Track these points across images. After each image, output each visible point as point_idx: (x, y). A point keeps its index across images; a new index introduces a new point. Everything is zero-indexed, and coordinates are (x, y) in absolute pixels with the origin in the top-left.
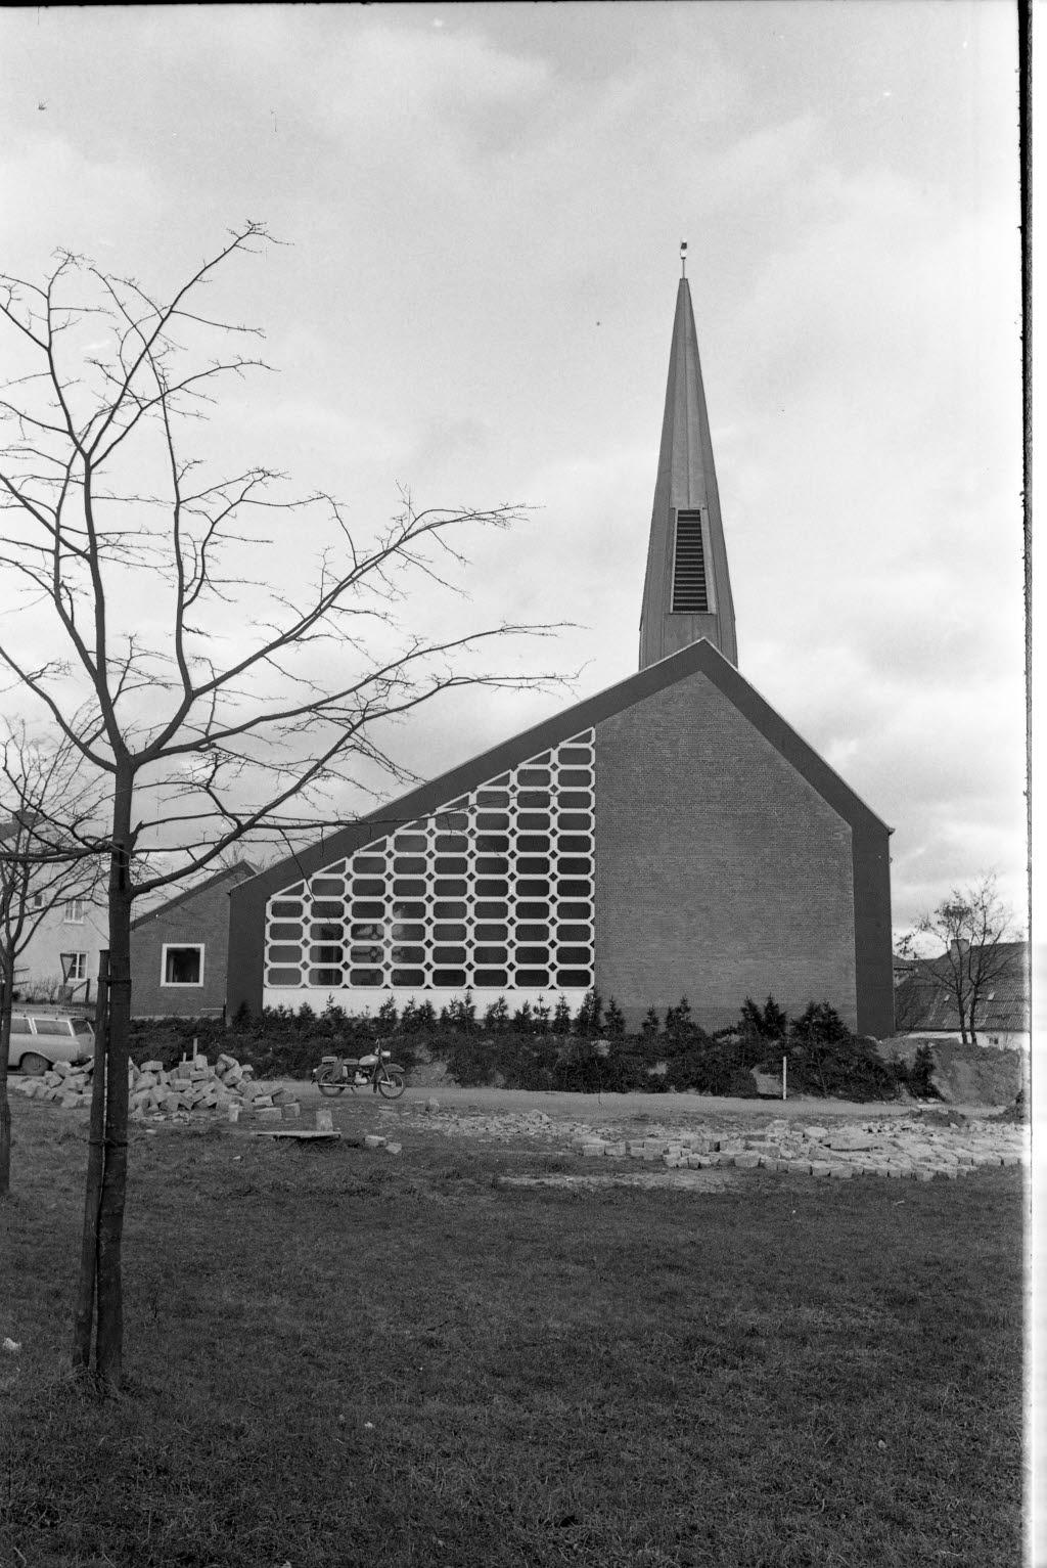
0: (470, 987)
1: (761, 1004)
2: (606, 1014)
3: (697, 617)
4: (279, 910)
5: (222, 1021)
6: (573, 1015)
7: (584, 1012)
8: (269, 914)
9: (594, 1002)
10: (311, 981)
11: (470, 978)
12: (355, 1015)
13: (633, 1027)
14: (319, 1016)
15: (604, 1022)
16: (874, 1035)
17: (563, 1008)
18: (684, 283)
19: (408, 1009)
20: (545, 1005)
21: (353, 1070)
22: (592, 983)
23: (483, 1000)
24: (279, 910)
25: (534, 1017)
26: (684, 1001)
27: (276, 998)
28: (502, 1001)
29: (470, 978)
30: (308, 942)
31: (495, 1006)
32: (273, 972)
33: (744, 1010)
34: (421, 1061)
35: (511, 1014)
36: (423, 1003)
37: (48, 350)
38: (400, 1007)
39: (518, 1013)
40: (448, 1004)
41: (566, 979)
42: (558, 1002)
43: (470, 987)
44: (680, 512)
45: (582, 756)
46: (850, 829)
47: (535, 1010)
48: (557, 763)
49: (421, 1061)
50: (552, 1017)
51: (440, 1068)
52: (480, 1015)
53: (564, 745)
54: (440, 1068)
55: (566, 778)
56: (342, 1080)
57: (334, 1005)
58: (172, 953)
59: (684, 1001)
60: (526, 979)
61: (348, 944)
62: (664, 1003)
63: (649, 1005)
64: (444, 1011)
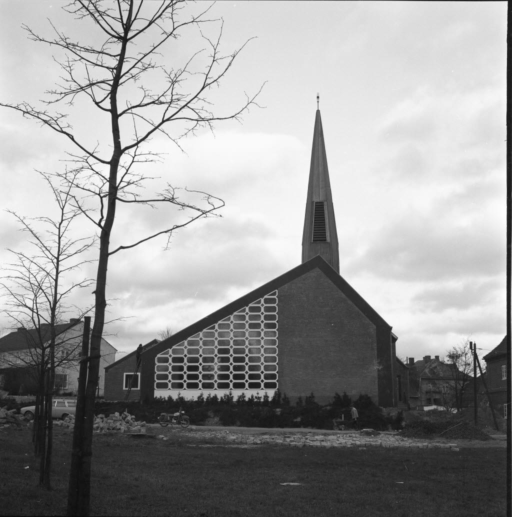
0: (231, 389)
1: (342, 394)
2: (282, 399)
3: (322, 244)
4: (160, 360)
5: (139, 402)
6: (270, 399)
7: (274, 398)
8: (156, 362)
9: (277, 395)
10: (219, 387)
11: (231, 385)
12: (189, 400)
13: (293, 404)
14: (175, 400)
15: (282, 402)
16: (441, 411)
17: (266, 397)
18: (318, 112)
19: (208, 397)
20: (260, 396)
21: (172, 417)
22: (277, 387)
23: (236, 394)
24: (160, 360)
25: (255, 400)
26: (312, 394)
27: (159, 393)
28: (243, 394)
29: (231, 385)
30: (170, 373)
31: (241, 396)
32: (158, 384)
33: (335, 397)
34: (210, 417)
35: (247, 399)
36: (214, 395)
37: (174, 29)
38: (205, 397)
39: (249, 399)
40: (223, 395)
41: (268, 386)
42: (264, 394)
43: (231, 389)
44: (316, 203)
45: (273, 301)
46: (375, 327)
47: (256, 397)
48: (264, 304)
49: (210, 417)
50: (262, 400)
51: (216, 419)
52: (235, 399)
53: (266, 297)
54: (216, 419)
55: (267, 309)
56: (168, 421)
57: (181, 396)
58: (127, 375)
59: (312, 394)
60: (253, 386)
61: (201, 373)
62: (305, 395)
63: (299, 395)
64: (222, 398)
